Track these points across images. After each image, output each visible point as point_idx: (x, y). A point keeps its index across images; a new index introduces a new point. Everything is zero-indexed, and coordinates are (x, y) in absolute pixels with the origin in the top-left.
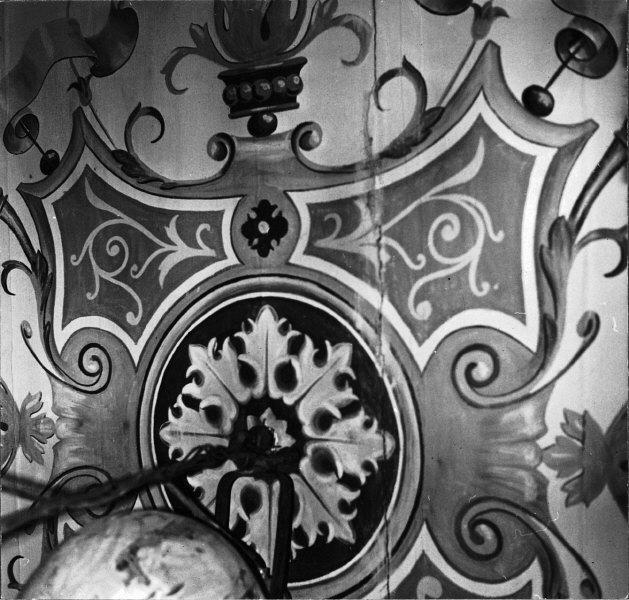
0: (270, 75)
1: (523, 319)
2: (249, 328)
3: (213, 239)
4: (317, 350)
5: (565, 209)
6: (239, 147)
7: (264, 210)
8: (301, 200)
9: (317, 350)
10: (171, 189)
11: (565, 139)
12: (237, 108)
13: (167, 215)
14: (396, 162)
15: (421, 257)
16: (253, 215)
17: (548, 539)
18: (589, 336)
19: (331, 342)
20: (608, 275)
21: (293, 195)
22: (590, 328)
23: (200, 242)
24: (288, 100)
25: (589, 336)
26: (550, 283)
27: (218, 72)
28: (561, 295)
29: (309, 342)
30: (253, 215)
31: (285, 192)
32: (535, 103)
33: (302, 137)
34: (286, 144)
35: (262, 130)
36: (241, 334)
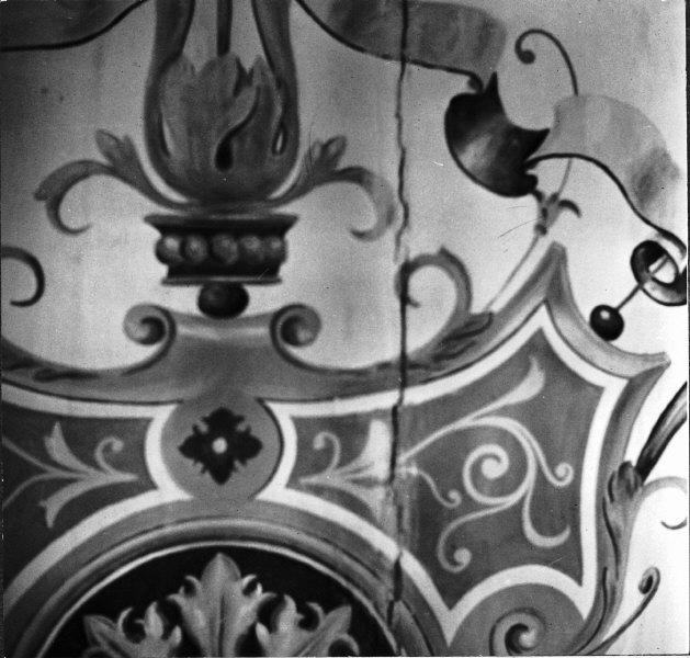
0: (239, 231)
1: (578, 578)
2: (190, 590)
3: (134, 457)
4: (531, 172)
5: (633, 454)
6: (182, 330)
7: (223, 421)
8: (285, 413)
9: (531, 172)
10: (75, 378)
11: (633, 370)
12: (179, 272)
13: (48, 419)
14: (445, 334)
15: (454, 495)
16: (204, 428)
17: (475, 352)
18: (647, 594)
19: (322, 604)
20: (664, 524)
21: (276, 408)
22: (649, 586)
23: (102, 463)
24: (268, 270)
25: (647, 594)
26: (613, 541)
27: (146, 212)
28: (622, 547)
29: (291, 604)
30: (204, 428)
31: (261, 401)
32: (608, 325)
33: (291, 324)
34: (262, 331)
35: (225, 305)
36: (179, 598)
